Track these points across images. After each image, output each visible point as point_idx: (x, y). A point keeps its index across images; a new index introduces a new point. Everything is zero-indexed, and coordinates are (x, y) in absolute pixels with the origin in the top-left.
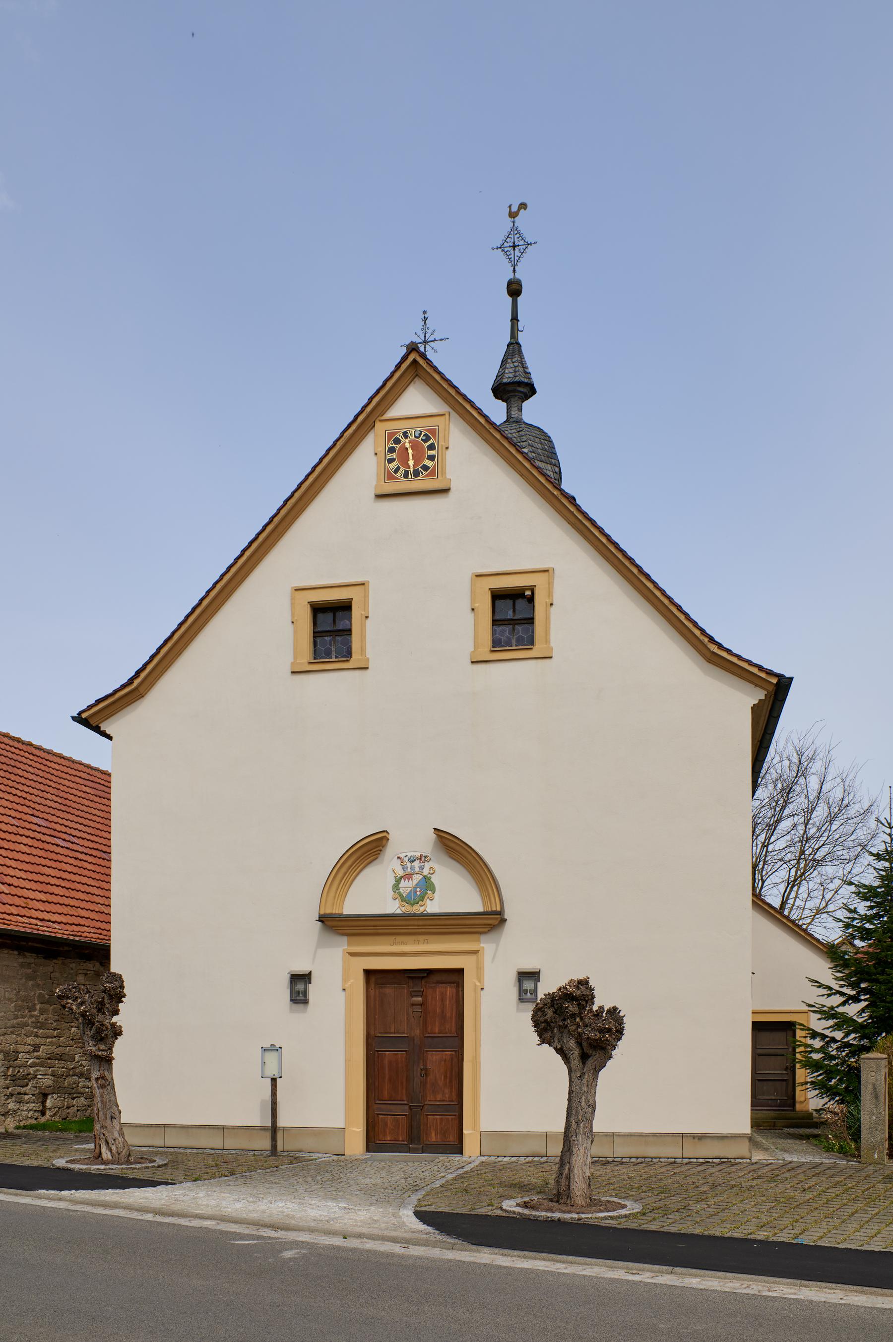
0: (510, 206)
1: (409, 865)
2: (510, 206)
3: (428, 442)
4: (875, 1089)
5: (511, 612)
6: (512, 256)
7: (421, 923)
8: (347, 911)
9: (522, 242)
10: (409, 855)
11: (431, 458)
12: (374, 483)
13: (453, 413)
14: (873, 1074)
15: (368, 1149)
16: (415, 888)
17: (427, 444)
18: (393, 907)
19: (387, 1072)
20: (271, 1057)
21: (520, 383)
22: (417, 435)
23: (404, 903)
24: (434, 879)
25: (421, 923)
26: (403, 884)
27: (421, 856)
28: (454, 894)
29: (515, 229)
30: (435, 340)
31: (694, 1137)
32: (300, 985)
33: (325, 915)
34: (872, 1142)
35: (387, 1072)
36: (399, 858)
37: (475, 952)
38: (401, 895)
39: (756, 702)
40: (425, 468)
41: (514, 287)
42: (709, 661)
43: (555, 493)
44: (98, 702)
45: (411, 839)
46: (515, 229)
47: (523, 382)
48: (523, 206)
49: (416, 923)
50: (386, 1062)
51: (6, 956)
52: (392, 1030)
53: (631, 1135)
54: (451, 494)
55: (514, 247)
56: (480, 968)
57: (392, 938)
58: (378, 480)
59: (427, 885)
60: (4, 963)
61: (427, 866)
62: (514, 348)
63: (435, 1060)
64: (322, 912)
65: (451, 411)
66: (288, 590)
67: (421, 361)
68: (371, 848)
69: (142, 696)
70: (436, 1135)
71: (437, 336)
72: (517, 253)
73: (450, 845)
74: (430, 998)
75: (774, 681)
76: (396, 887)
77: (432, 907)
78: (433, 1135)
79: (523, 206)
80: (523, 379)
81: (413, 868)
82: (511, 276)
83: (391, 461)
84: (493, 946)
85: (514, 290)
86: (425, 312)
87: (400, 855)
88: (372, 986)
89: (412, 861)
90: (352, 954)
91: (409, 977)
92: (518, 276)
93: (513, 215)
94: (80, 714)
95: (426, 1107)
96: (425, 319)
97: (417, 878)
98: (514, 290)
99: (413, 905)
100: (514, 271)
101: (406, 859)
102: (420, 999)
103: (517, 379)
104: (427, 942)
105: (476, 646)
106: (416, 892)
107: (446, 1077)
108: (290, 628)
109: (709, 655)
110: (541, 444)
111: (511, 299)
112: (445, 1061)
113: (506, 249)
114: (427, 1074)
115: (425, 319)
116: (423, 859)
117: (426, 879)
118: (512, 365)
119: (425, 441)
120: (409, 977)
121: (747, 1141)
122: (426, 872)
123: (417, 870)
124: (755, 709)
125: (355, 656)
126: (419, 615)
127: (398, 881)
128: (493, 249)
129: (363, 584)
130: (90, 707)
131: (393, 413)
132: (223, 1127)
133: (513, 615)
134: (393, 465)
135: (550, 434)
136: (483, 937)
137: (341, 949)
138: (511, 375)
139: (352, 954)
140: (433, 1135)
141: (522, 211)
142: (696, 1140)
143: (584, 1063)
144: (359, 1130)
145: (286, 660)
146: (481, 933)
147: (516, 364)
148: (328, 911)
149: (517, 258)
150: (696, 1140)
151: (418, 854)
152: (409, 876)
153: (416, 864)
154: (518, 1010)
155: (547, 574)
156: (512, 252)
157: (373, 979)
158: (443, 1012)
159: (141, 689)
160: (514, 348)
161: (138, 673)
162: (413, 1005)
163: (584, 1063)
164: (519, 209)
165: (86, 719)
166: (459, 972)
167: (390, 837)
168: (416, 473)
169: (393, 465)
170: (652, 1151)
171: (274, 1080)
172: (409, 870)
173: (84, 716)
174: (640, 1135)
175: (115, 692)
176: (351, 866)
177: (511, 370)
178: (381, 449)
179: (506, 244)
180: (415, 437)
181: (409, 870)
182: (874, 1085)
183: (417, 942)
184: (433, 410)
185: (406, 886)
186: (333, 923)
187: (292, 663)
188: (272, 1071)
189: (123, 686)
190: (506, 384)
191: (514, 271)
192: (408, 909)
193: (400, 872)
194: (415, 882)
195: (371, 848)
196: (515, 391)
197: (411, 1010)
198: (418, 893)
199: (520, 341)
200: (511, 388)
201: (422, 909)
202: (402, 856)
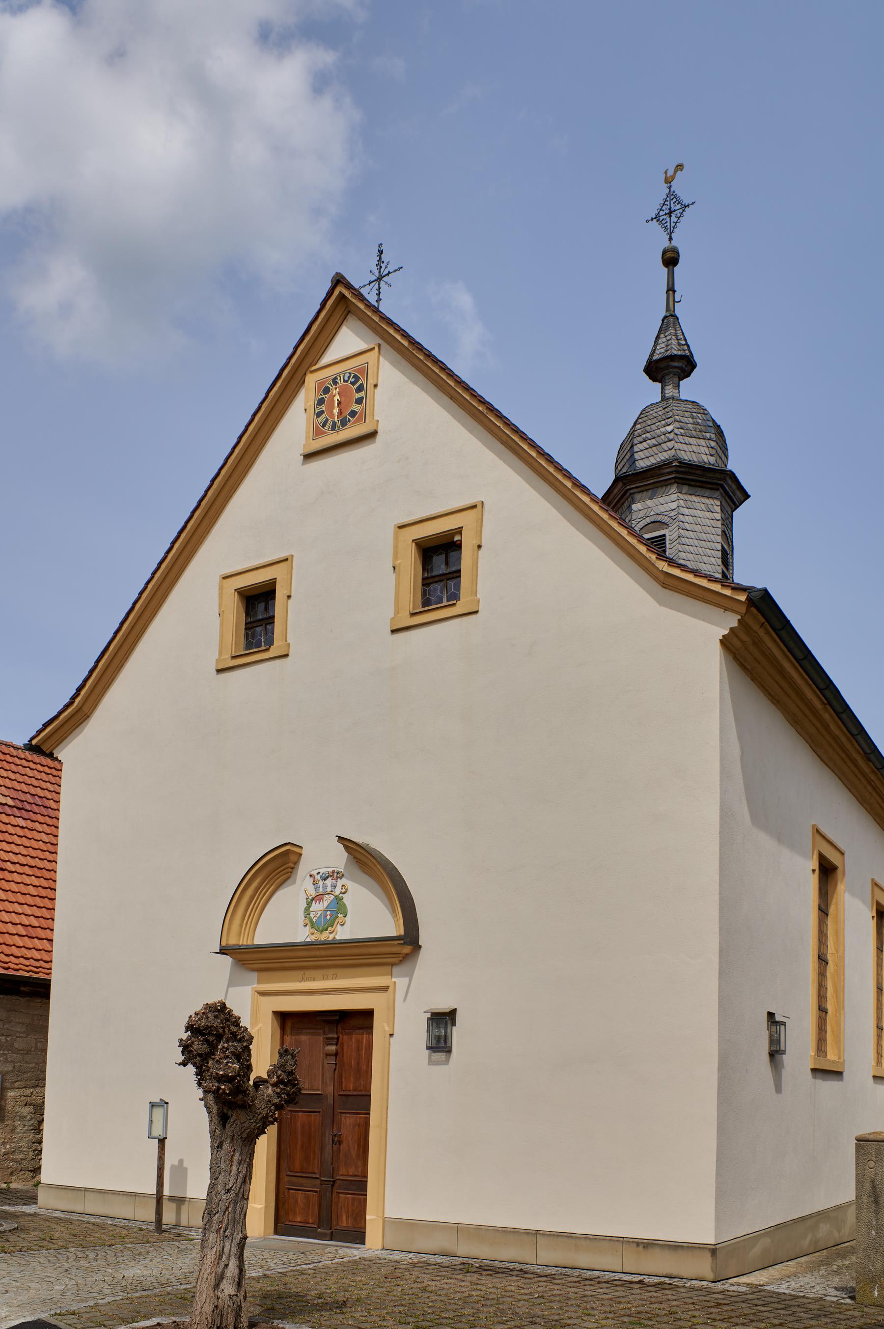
0: (666, 172)
1: (321, 883)
2: (666, 172)
3: (358, 382)
4: (874, 1187)
5: (443, 566)
6: (668, 224)
7: (323, 953)
8: (260, 939)
9: (679, 206)
10: (322, 871)
11: (359, 401)
12: (303, 442)
13: (384, 345)
14: (872, 1164)
15: (276, 1232)
17: (356, 387)
18: (303, 935)
19: (299, 1137)
20: (158, 1113)
21: (672, 358)
22: (346, 378)
23: (313, 930)
24: (347, 900)
25: (323, 953)
26: (315, 907)
28: (368, 916)
29: (671, 195)
30: (389, 273)
31: (638, 1244)
33: (227, 946)
34: (870, 1271)
35: (299, 1137)
37: (385, 989)
39: (726, 632)
40: (353, 414)
41: (669, 255)
42: (664, 586)
43: (480, 408)
44: (46, 725)
46: (671, 195)
47: (676, 355)
48: (680, 167)
49: (318, 953)
50: (299, 1124)
51: (39, 1005)
52: (307, 1087)
53: (557, 1235)
54: (379, 437)
55: (670, 214)
56: (391, 1009)
57: (300, 973)
58: (307, 438)
59: (339, 908)
60: (36, 1013)
61: (340, 883)
62: (670, 320)
63: (348, 1122)
64: (224, 944)
65: (381, 342)
66: (217, 579)
67: (347, 294)
68: (279, 866)
69: (87, 717)
70: (347, 1218)
71: (391, 268)
72: (674, 219)
73: (364, 859)
74: (345, 1047)
75: (743, 597)
76: (307, 910)
77: (342, 933)
78: (344, 1218)
79: (680, 167)
80: (675, 352)
81: (325, 887)
82: (666, 244)
83: (319, 415)
84: (406, 980)
85: (671, 260)
86: (380, 245)
88: (288, 1030)
90: (263, 994)
91: (325, 1021)
92: (674, 243)
93: (668, 181)
94: (30, 741)
95: (338, 1182)
96: (381, 252)
97: (328, 899)
98: (671, 260)
99: (322, 932)
100: (670, 239)
102: (334, 1048)
103: (668, 353)
104: (335, 977)
105: (397, 612)
107: (359, 1145)
108: (217, 620)
109: (661, 577)
110: (693, 418)
111: (666, 269)
112: (359, 1125)
113: (661, 218)
114: (340, 1142)
115: (381, 252)
116: (336, 875)
117: (338, 899)
118: (664, 340)
119: (353, 383)
120: (325, 1021)
121: (708, 1255)
124: (725, 642)
125: (276, 643)
126: (349, 587)
128: (647, 221)
129: (287, 560)
130: (40, 732)
131: (326, 360)
132: (136, 1194)
133: (439, 562)
134: (321, 419)
135: (706, 407)
136: (395, 969)
137: (250, 987)
138: (662, 350)
139: (263, 994)
140: (344, 1218)
141: (679, 172)
142: (641, 1247)
143: (224, 1126)
144: (259, 1206)
145: (211, 658)
146: (392, 965)
147: (668, 338)
149: (673, 225)
150: (641, 1247)
151: (330, 870)
152: (319, 897)
153: (329, 882)
154: (431, 1062)
155: (475, 510)
156: (668, 219)
157: (289, 1024)
158: (358, 1064)
159: (86, 709)
160: (670, 320)
161: (79, 690)
162: (327, 1055)
163: (224, 1126)
164: (675, 172)
165: (36, 745)
166: (367, 1015)
167: (304, 852)
168: (344, 423)
169: (321, 419)
170: (584, 1259)
171: (162, 1142)
172: (321, 889)
173: (34, 742)
174: (570, 1236)
175: (60, 713)
177: (663, 345)
178: (312, 403)
179: (662, 213)
180: (345, 381)
181: (321, 889)
182: (873, 1182)
183: (325, 978)
184: (364, 346)
186: (250, 959)
187: (217, 660)
188: (158, 1131)
189: (67, 707)
190: (658, 361)
191: (670, 239)
193: (312, 892)
194: (326, 904)
195: (279, 866)
196: (668, 367)
197: (326, 1061)
198: (328, 917)
199: (677, 313)
200: (663, 365)
201: (331, 937)
202: (314, 873)
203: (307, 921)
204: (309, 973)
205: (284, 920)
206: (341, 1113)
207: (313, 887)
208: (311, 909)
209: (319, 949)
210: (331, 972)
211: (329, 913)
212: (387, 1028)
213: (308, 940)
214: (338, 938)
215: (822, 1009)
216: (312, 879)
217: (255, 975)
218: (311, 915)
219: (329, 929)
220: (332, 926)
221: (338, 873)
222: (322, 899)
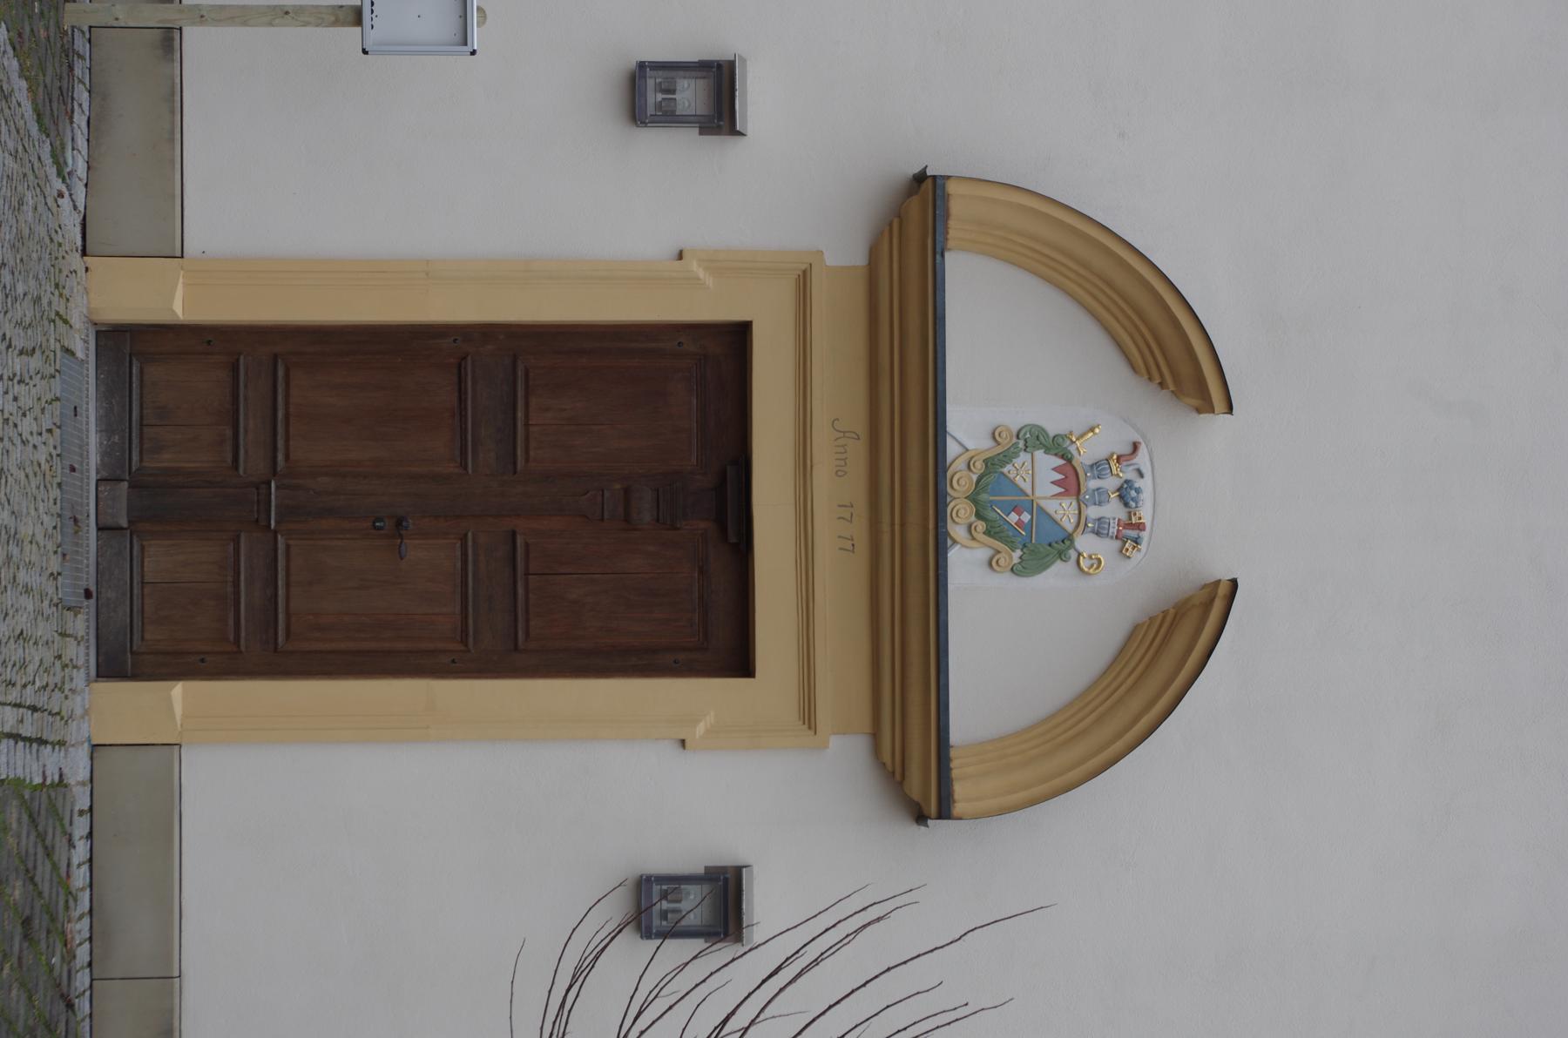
1: (1110, 483)
10: (1145, 484)
16: (1031, 506)
18: (968, 427)
23: (979, 467)
24: (1057, 576)
25: (914, 535)
26: (1047, 464)
27: (1140, 527)
28: (1011, 639)
32: (694, 96)
33: (946, 198)
36: (1135, 447)
37: (808, 717)
38: (1007, 457)
45: (1205, 495)
59: (1041, 548)
64: (952, 188)
73: (1182, 633)
76: (1035, 439)
77: (967, 565)
81: (1100, 497)
87: (1143, 450)
89: (1125, 494)
90: (803, 282)
97: (1064, 511)
99: (973, 498)
101: (1129, 474)
106: (1016, 509)
116: (1130, 533)
122: (1085, 543)
123: (1092, 512)
127: (1057, 446)
139: (803, 282)
146: (875, 736)
148: (955, 207)
151: (1145, 513)
152: (1070, 483)
153: (1113, 510)
172: (1093, 484)
176: (1110, 284)
181: (1093, 484)
185: (1037, 475)
192: (960, 481)
193: (1086, 452)
194: (1051, 506)
195: (1173, 357)
198: (1013, 518)
202: (1142, 459)
203: (1006, 442)
204: (858, 452)
205: (1010, 365)
206: (464, 539)
207: (1101, 453)
208: (1039, 454)
209: (926, 528)
210: (859, 529)
211: (1026, 517)
212: (701, 729)
213: (952, 449)
214: (954, 555)
215: (764, 981)
216: (1127, 449)
217: (859, 258)
218: (1024, 457)
219: (981, 526)
220: (988, 533)
221: (1137, 541)
222: (1066, 493)
